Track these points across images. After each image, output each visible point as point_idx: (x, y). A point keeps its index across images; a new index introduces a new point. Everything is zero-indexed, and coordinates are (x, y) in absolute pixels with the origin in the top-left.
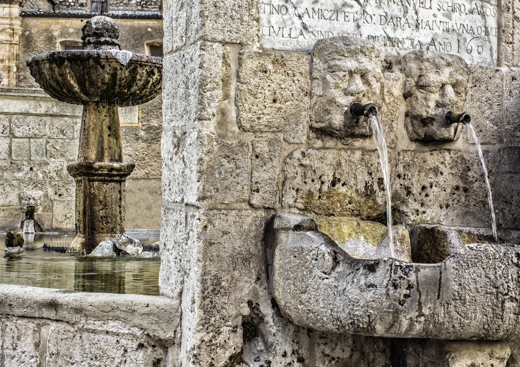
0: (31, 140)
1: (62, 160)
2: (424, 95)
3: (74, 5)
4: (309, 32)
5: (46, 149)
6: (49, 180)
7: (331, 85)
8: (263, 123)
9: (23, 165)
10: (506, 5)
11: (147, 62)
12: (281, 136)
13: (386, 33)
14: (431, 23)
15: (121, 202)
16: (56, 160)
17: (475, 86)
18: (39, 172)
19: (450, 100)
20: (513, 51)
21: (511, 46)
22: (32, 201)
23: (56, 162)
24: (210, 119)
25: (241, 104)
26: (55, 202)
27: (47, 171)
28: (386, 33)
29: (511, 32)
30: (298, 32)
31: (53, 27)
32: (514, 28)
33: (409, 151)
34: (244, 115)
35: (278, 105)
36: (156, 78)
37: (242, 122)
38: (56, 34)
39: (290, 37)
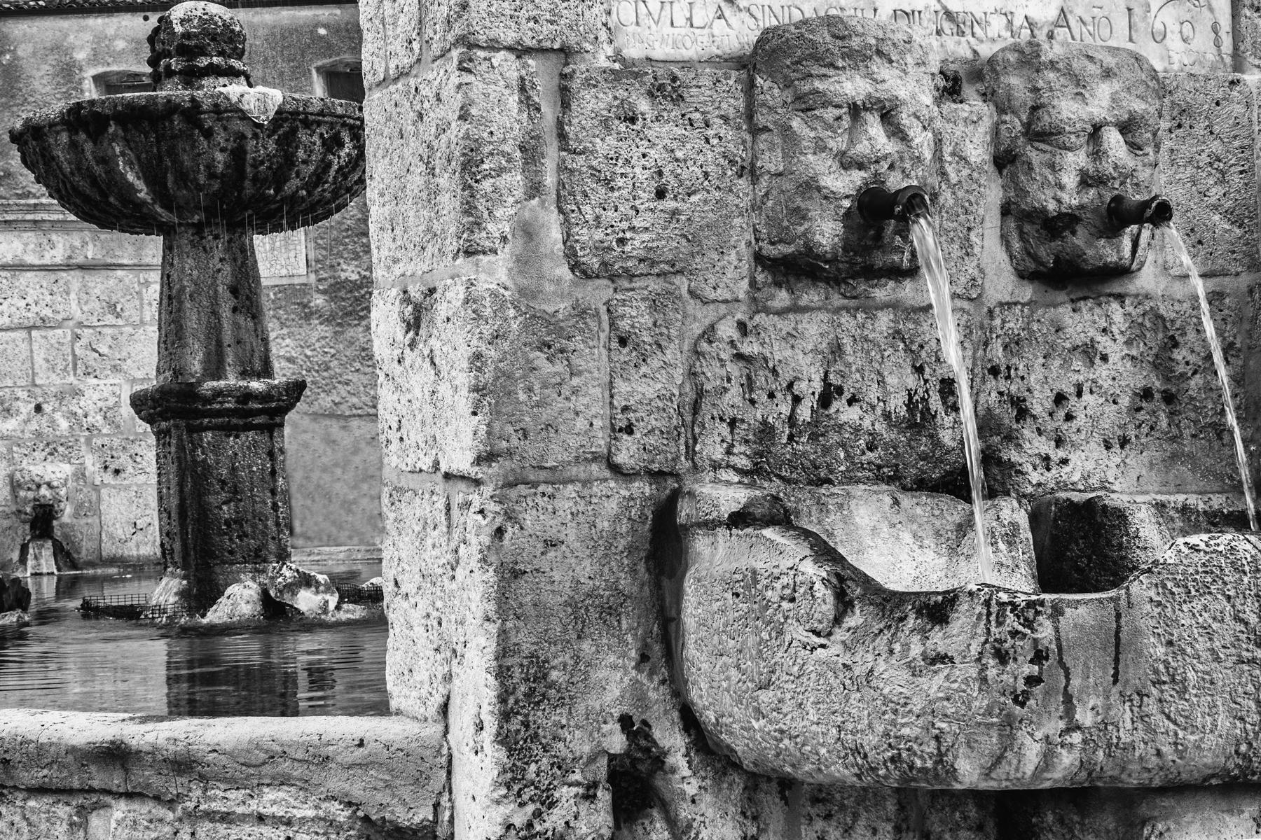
0: (34, 333)
1: (116, 381)
2: (1048, 156)
4: (740, 10)
5: (74, 355)
6: (87, 433)
7: (805, 143)
9: (18, 399)
11: (321, 113)
15: (275, 481)
16: (102, 382)
18: (58, 416)
27: (80, 412)
31: (71, 38)
33: (1016, 304)
35: (669, 204)
36: (348, 155)
38: (80, 56)
39: (692, 26)
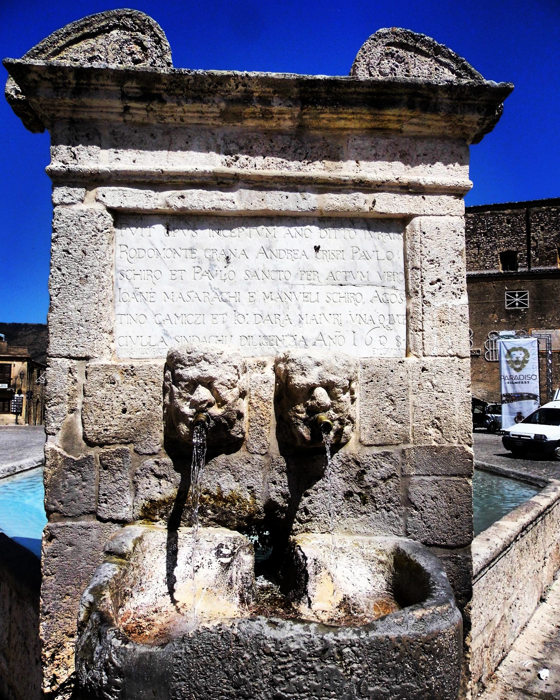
8: (111, 435)
10: (414, 289)
12: (130, 448)
13: (261, 332)
14: (317, 317)
17: (372, 381)
20: (423, 339)
21: (420, 333)
24: (54, 434)
25: (86, 417)
28: (261, 332)
29: (420, 318)
30: (159, 339)
32: (423, 314)
34: (89, 428)
37: (88, 435)
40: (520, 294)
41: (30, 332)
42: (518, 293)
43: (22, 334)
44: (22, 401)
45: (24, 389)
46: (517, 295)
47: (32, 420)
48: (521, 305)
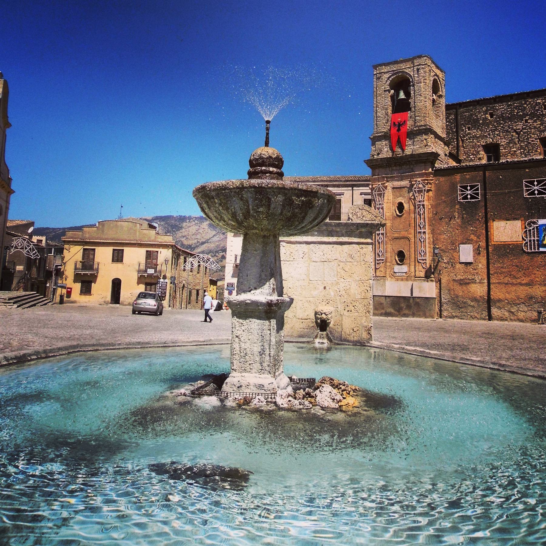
3: (474, 159)
6: (340, 297)
16: (345, 281)
19: (224, 488)
22: (324, 316)
23: (345, 282)
26: (344, 317)
27: (338, 290)
40: (472, 187)
41: (194, 223)
42: (537, 181)
43: (186, 225)
44: (166, 286)
45: (168, 275)
46: (536, 183)
47: (178, 304)
48: (472, 197)
